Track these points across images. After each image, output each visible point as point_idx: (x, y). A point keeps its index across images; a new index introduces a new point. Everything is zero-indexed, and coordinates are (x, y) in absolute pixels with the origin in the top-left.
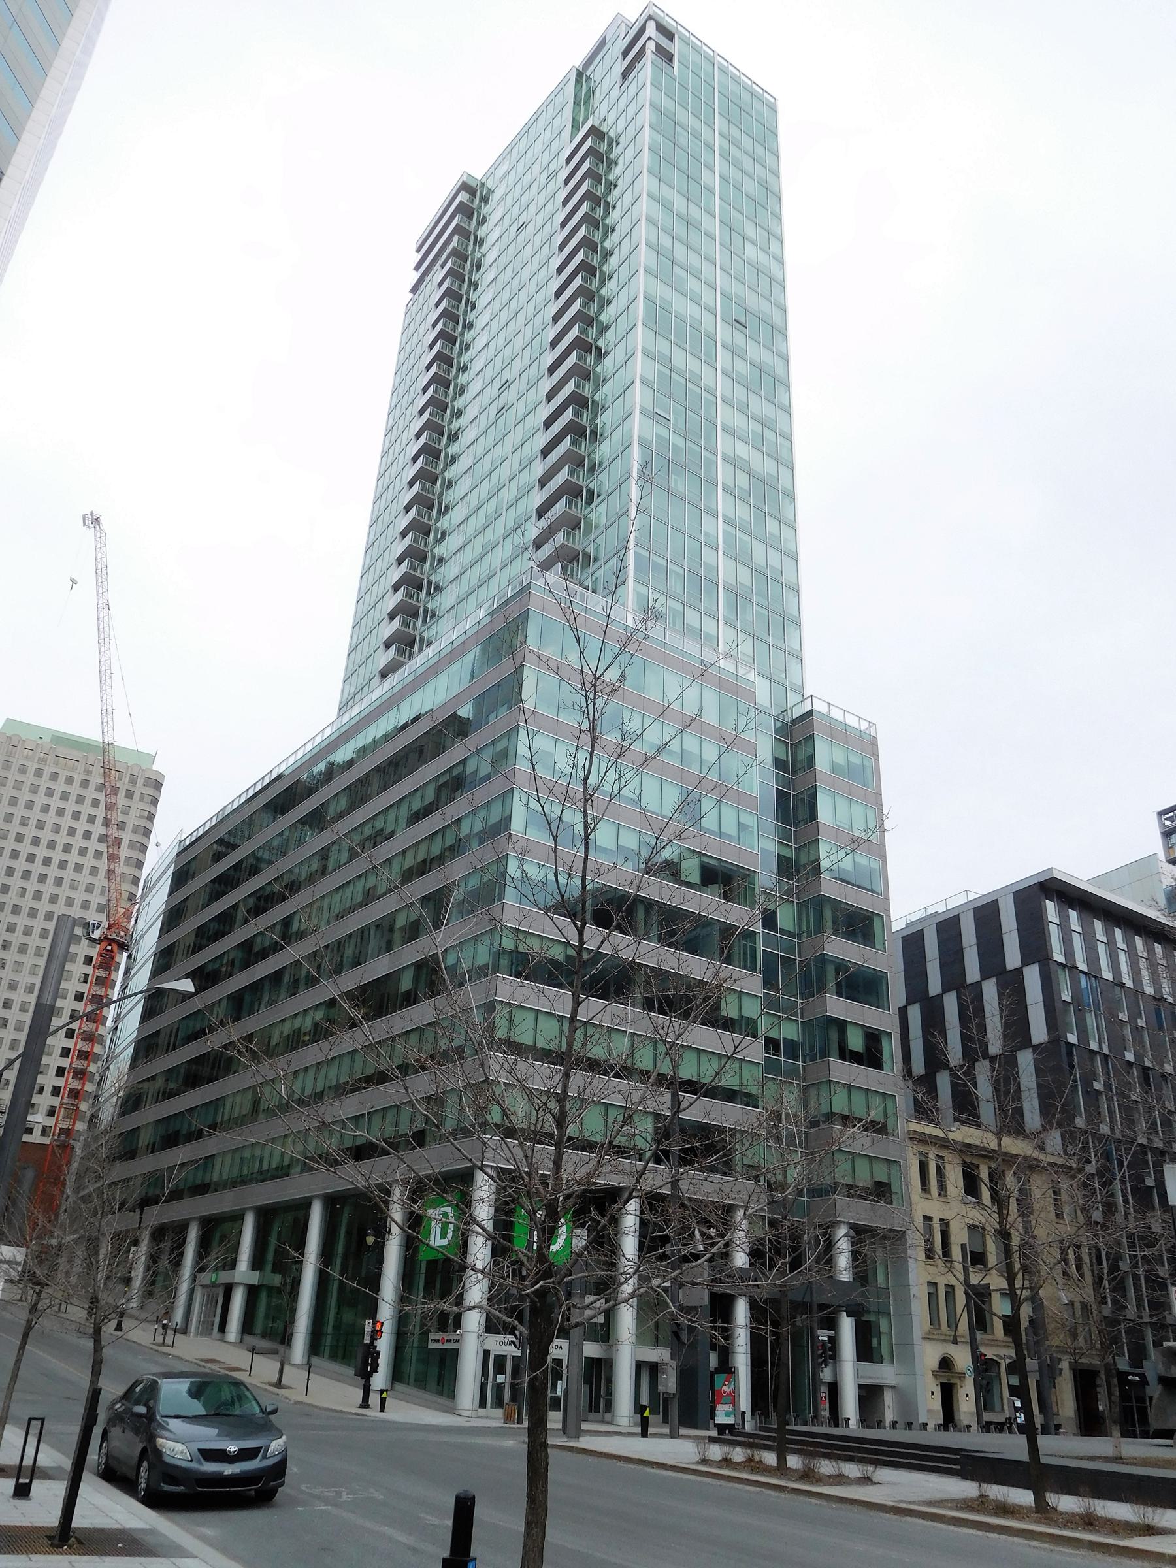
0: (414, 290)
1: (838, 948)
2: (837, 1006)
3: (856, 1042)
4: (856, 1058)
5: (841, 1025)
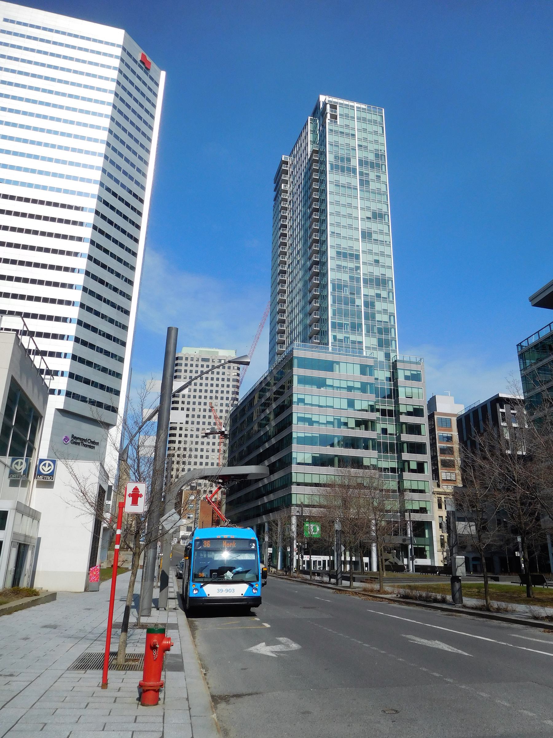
0: (275, 200)
1: (406, 437)
2: (406, 456)
3: (413, 466)
4: (413, 471)
5: (408, 462)
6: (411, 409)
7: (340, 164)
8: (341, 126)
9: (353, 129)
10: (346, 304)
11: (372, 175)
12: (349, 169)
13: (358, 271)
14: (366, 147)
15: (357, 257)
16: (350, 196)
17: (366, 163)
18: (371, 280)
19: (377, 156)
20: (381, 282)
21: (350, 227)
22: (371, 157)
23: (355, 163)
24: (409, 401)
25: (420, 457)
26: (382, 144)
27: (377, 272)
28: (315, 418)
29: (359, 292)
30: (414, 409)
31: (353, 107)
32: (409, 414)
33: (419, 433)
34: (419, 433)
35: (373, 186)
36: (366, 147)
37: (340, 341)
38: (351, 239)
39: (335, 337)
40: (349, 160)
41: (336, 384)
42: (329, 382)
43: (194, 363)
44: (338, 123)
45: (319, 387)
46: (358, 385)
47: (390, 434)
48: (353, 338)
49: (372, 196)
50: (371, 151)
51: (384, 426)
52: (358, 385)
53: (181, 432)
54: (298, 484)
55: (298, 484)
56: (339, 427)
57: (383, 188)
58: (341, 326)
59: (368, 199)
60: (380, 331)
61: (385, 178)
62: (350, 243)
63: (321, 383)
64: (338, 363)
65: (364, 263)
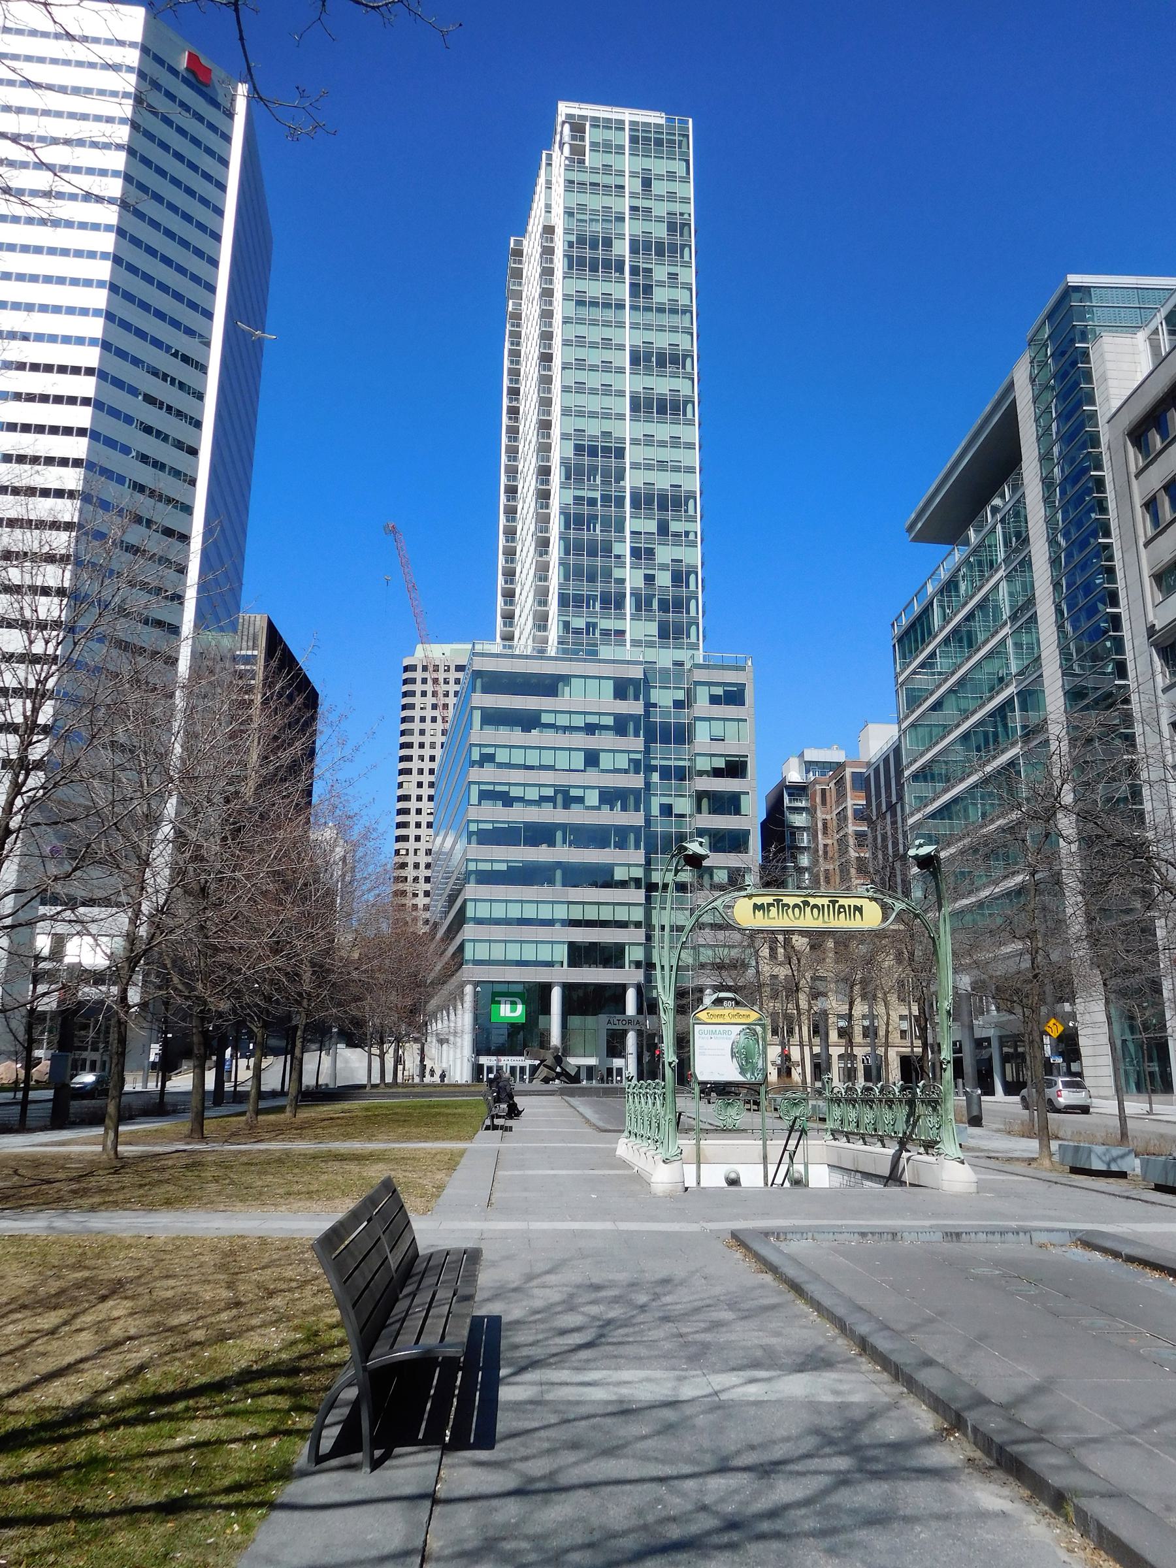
3: (721, 877)
6: (720, 763)
7: (588, 253)
8: (594, 171)
9: (621, 173)
10: (592, 553)
11: (660, 273)
12: (607, 264)
13: (622, 483)
14: (648, 210)
15: (620, 453)
16: (607, 324)
17: (647, 246)
18: (649, 500)
19: (672, 227)
20: (670, 503)
21: (607, 390)
22: (660, 231)
23: (622, 248)
24: (718, 748)
25: (732, 860)
26: (685, 201)
27: (663, 481)
28: (515, 792)
29: (620, 529)
30: (727, 762)
31: (623, 122)
32: (717, 773)
33: (737, 812)
34: (737, 812)
35: (661, 295)
36: (648, 210)
37: (577, 631)
38: (607, 416)
39: (566, 625)
40: (608, 243)
41: (563, 720)
42: (546, 719)
43: (441, 676)
44: (587, 164)
45: (527, 729)
46: (609, 721)
47: (678, 816)
48: (605, 624)
49: (666, 319)
50: (660, 219)
51: (666, 800)
52: (609, 721)
53: (419, 818)
54: (480, 921)
55: (480, 921)
56: (566, 806)
57: (682, 297)
58: (579, 601)
59: (648, 327)
60: (664, 606)
61: (690, 276)
62: (607, 425)
63: (529, 721)
64: (566, 679)
65: (635, 466)
